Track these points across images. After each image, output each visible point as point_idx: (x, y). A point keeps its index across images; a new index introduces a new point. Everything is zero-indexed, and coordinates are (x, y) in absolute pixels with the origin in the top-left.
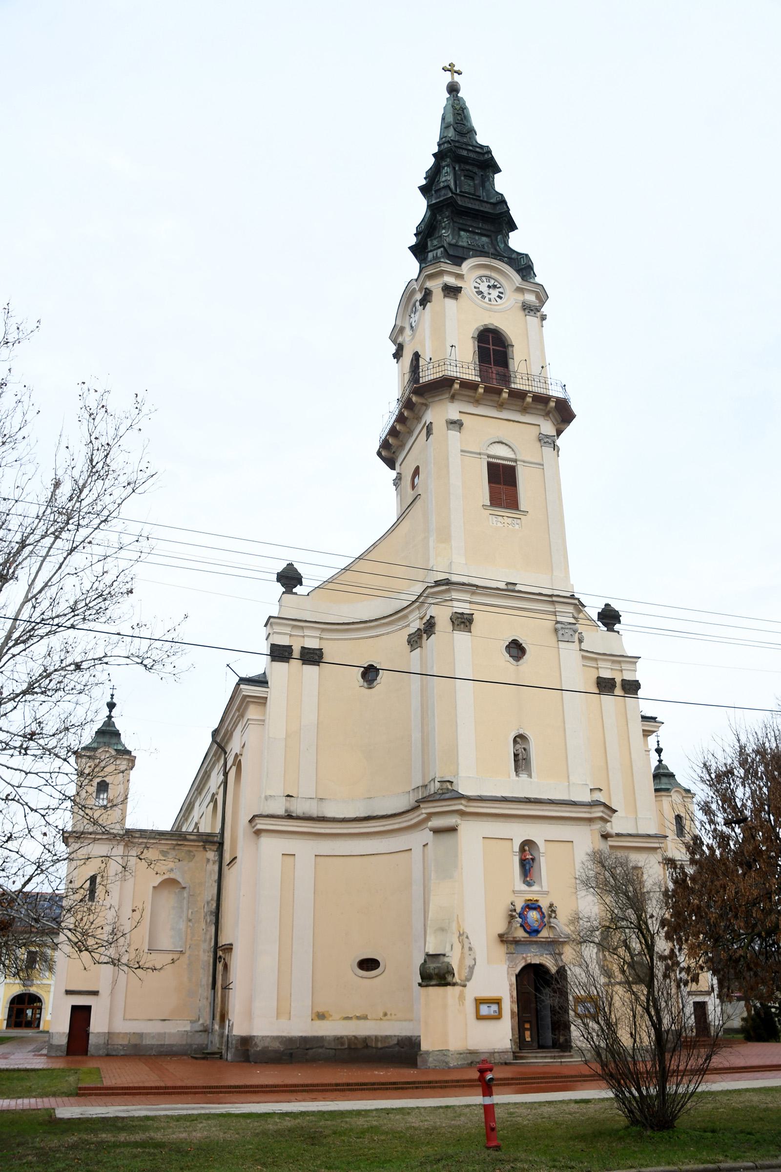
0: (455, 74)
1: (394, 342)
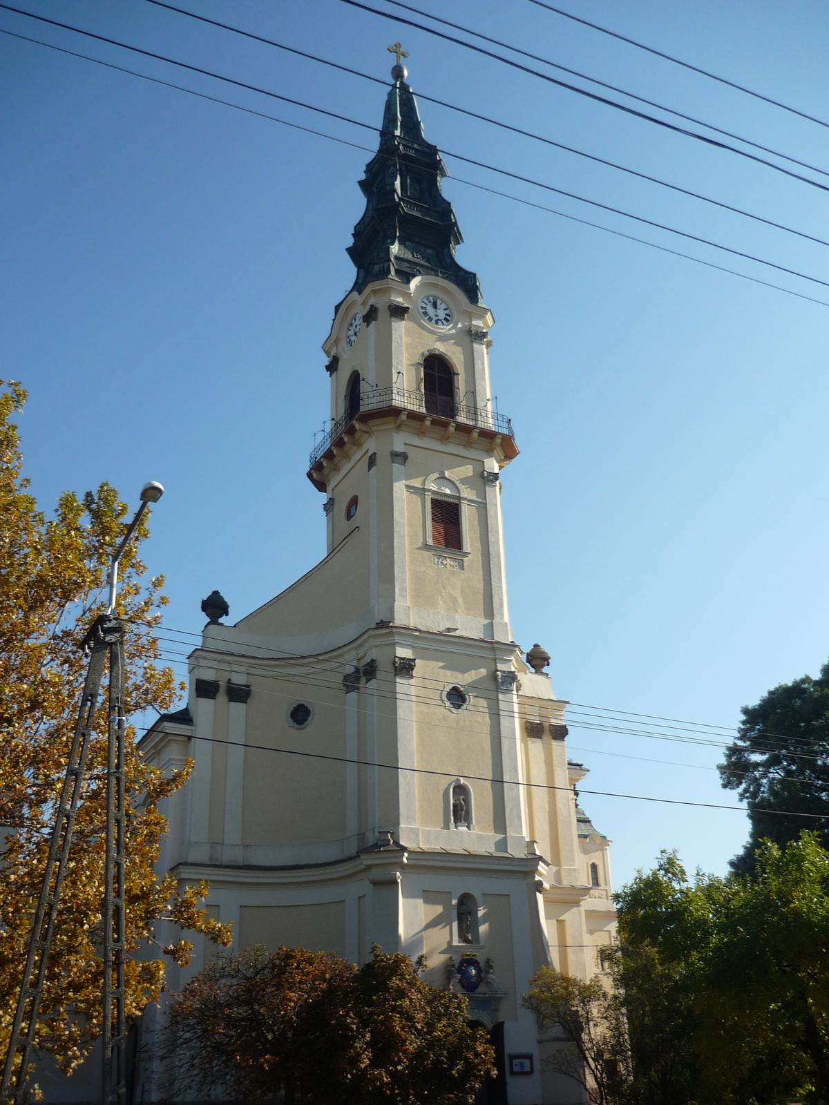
0: (401, 56)
1: (328, 353)
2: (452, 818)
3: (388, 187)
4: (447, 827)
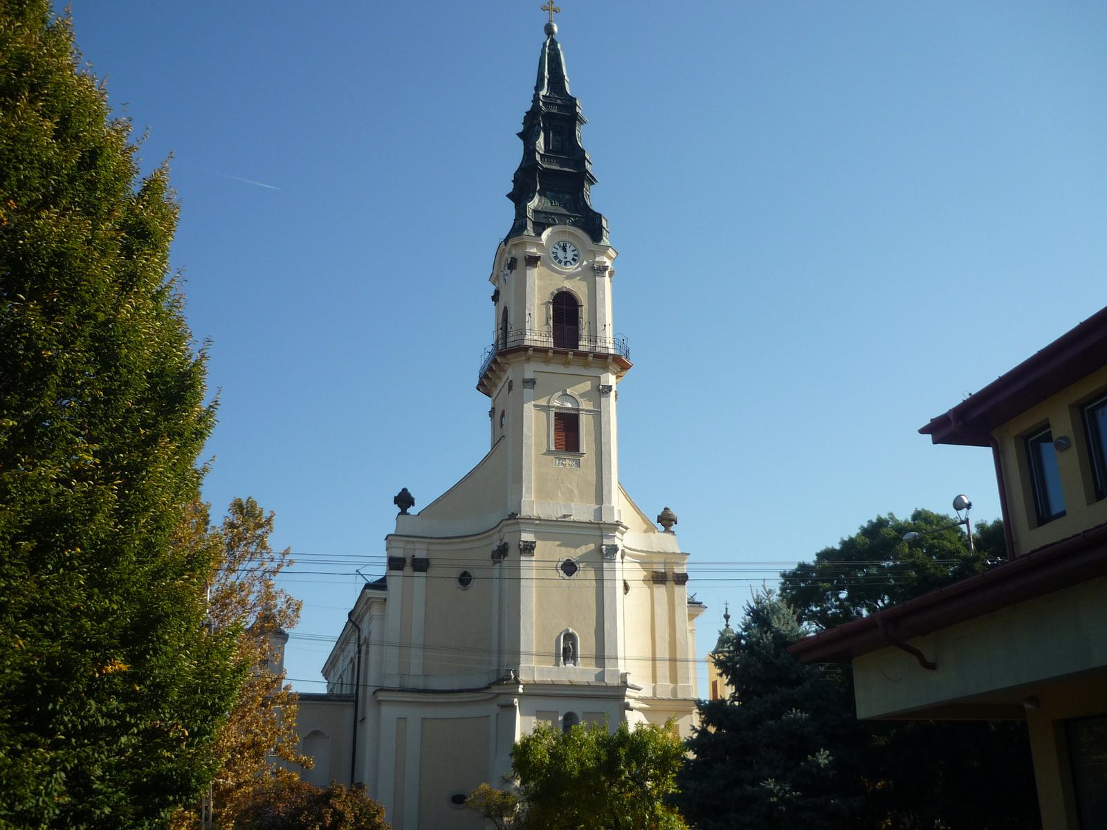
2: (562, 658)
3: (531, 147)
4: (557, 664)
